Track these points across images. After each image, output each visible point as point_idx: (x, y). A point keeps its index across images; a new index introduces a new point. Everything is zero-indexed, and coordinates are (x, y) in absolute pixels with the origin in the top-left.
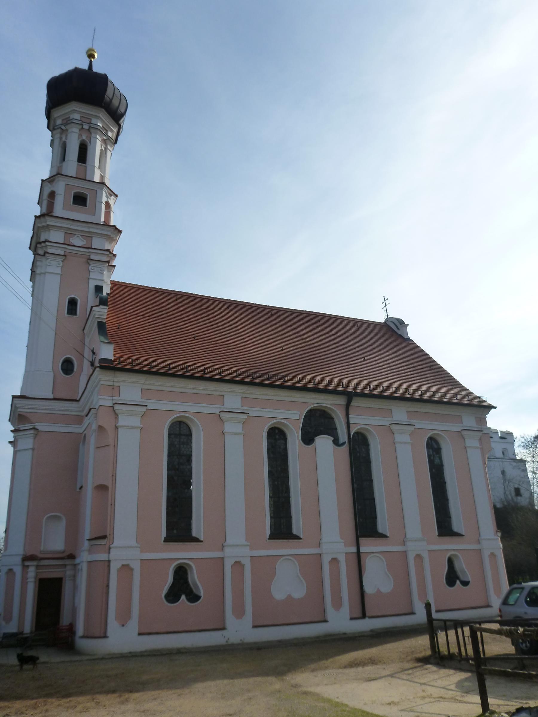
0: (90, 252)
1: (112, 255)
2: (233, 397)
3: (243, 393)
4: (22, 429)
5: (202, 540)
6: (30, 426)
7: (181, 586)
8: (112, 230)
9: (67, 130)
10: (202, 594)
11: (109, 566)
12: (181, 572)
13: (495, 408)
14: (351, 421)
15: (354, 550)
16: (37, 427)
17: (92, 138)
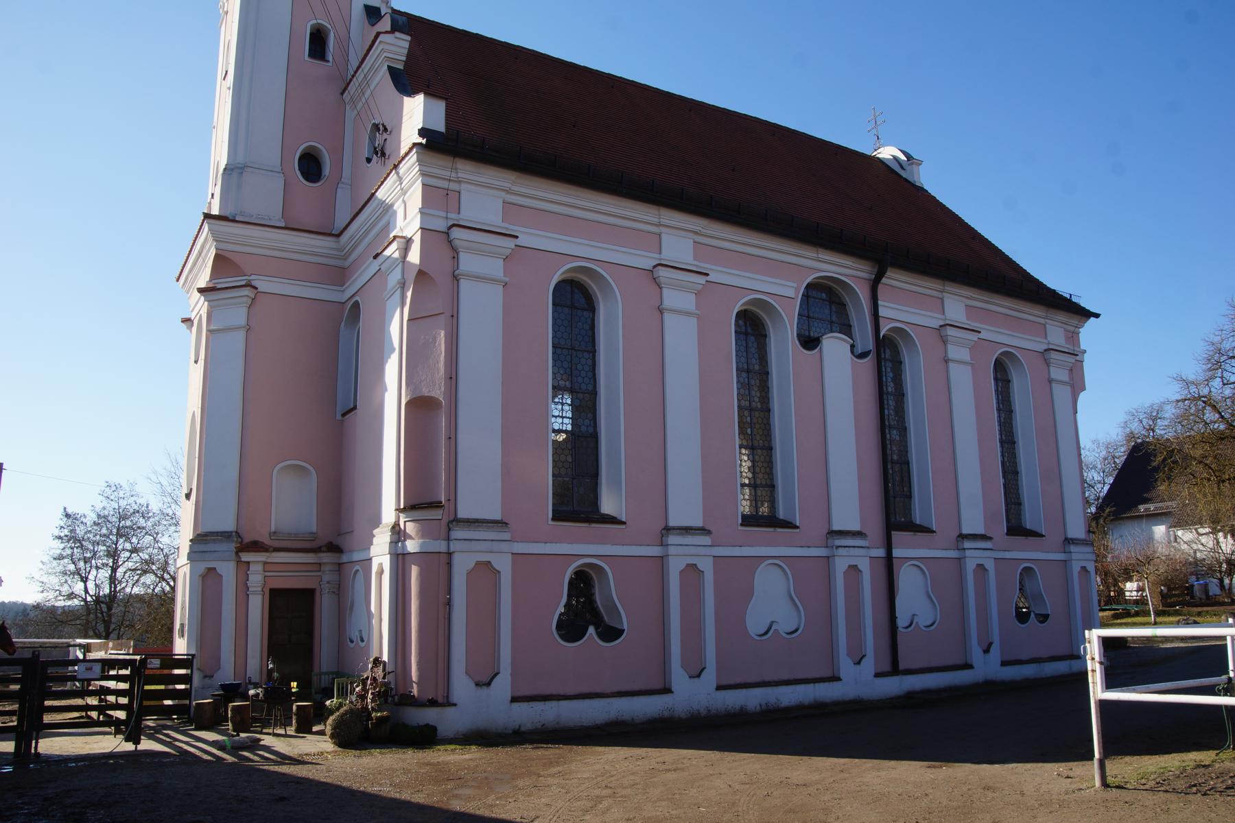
2: (679, 237)
3: (696, 233)
6: (241, 281)
7: (584, 611)
10: (625, 627)
11: (449, 564)
12: (583, 582)
13: (1097, 316)
14: (882, 312)
15: (881, 552)
16: (254, 283)
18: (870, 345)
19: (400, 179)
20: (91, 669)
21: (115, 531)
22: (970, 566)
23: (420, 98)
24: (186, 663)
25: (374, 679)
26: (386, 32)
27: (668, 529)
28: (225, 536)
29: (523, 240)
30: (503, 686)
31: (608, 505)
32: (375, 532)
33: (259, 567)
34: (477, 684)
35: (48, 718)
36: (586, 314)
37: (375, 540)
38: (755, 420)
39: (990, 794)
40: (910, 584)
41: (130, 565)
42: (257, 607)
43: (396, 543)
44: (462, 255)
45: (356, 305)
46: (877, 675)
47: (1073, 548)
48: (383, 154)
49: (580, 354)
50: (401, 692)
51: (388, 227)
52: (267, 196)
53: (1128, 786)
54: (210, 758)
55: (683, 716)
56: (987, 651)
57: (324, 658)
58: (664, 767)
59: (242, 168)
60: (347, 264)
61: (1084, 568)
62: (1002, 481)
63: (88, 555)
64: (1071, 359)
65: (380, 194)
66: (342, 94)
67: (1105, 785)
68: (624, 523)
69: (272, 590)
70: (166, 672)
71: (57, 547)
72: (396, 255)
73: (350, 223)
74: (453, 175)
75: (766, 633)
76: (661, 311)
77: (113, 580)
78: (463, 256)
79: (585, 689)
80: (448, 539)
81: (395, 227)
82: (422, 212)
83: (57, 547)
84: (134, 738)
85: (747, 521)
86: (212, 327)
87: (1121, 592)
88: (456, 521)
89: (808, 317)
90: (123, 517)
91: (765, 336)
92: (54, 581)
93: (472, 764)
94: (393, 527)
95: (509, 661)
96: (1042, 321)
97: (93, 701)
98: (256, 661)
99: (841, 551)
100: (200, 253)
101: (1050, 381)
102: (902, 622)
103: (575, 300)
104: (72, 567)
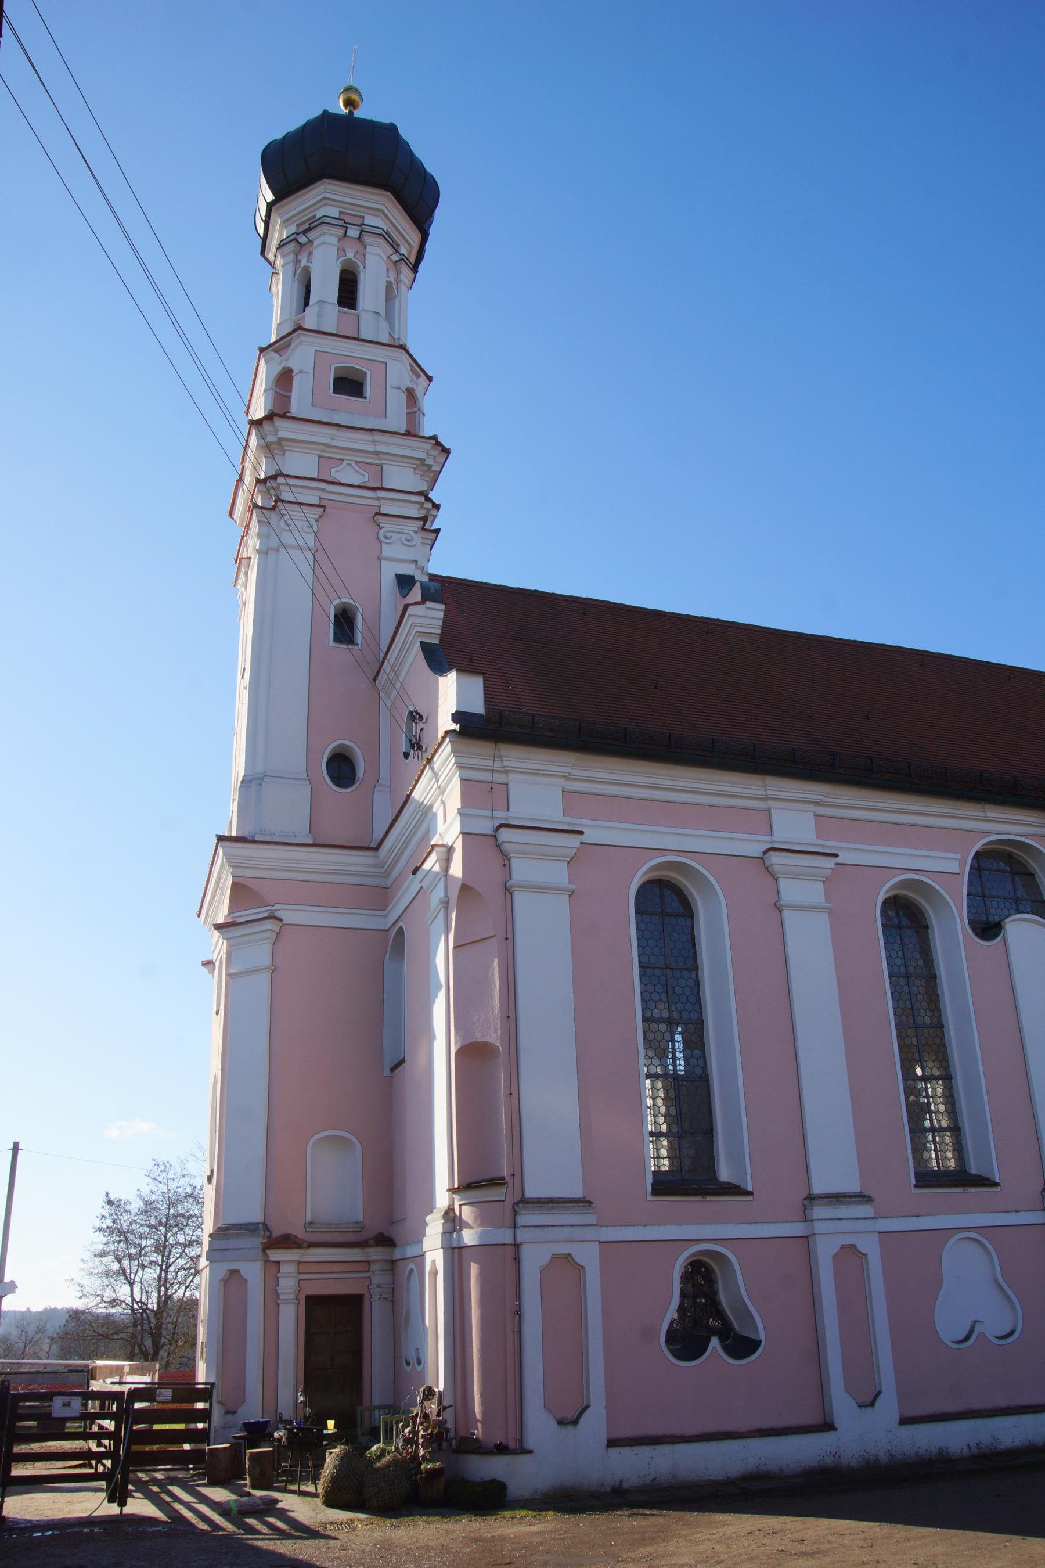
0: (378, 499)
1: (430, 506)
2: (796, 812)
3: (817, 804)
5: (750, 1189)
6: (262, 912)
7: (704, 1318)
8: (429, 446)
9: (310, 242)
10: (762, 1337)
11: (517, 1259)
12: (701, 1277)
17: (367, 256)
19: (436, 775)
21: (164, 1220)
23: (453, 676)
24: (206, 1395)
25: (426, 1416)
27: (811, 1198)
28: (250, 1228)
29: (593, 834)
30: (595, 1425)
31: (725, 1174)
32: (428, 1218)
34: (561, 1422)
35: (18, 1470)
36: (681, 921)
37: (428, 1229)
38: (923, 1041)
42: (290, 1319)
43: (451, 1233)
44: (514, 861)
45: (401, 931)
48: (420, 747)
49: (677, 974)
50: (462, 1434)
51: (428, 834)
52: (291, 809)
54: (206, 1527)
55: (854, 1463)
58: (802, 1548)
59: (262, 779)
63: (133, 1251)
65: (416, 795)
66: (375, 680)
68: (750, 1193)
69: (308, 1298)
70: (185, 1406)
71: (99, 1241)
72: (437, 868)
74: (497, 764)
75: (967, 1338)
76: (779, 909)
77: (162, 1282)
78: (515, 863)
79: (711, 1427)
80: (515, 1227)
82: (461, 813)
83: (99, 1241)
84: (118, 1495)
85: (663, 1185)
86: (232, 971)
88: (524, 1202)
89: (984, 896)
90: (171, 1204)
91: (927, 927)
93: (536, 1539)
94: (446, 1213)
98: (291, 1397)
100: (217, 883)
103: (666, 905)
104: (116, 1266)
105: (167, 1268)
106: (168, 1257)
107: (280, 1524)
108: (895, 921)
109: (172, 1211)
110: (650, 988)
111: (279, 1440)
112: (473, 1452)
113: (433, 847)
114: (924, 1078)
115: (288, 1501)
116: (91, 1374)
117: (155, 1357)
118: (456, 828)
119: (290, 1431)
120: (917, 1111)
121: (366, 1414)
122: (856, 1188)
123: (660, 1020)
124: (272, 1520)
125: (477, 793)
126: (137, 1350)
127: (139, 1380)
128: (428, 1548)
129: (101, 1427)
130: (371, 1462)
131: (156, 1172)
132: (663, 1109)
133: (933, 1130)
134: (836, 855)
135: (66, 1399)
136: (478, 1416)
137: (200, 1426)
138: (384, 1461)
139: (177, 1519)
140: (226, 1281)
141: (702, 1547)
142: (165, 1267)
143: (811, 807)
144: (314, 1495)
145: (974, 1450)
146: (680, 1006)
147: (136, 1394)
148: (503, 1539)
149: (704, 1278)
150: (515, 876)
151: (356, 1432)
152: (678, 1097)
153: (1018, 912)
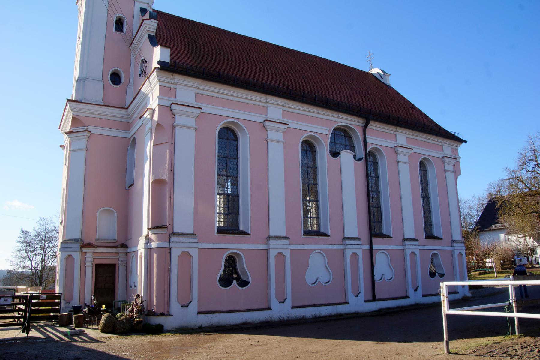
2: (276, 108)
3: (283, 106)
4: (74, 131)
7: (231, 274)
10: (250, 281)
11: (170, 253)
12: (231, 261)
13: (466, 142)
14: (368, 140)
15: (368, 247)
16: (89, 130)
18: (363, 155)
19: (150, 83)
20: (7, 300)
22: (408, 253)
24: (59, 297)
25: (137, 304)
26: (147, 19)
27: (269, 237)
28: (76, 241)
29: (204, 110)
30: (194, 307)
31: (241, 228)
33: (91, 255)
34: (182, 306)
36: (234, 142)
38: (310, 189)
39: (397, 357)
40: (380, 260)
41: (50, 253)
42: (90, 273)
44: (176, 116)
45: (134, 139)
46: (366, 301)
47: (455, 244)
48: (145, 73)
49: (231, 160)
50: (149, 309)
51: (146, 104)
52: (96, 91)
53: (460, 353)
54: (59, 340)
55: (276, 320)
56: (416, 290)
57: (120, 294)
58: (258, 344)
59: (85, 79)
60: (131, 121)
61: (460, 253)
62: (423, 215)
63: (32, 249)
64: (455, 161)
65: (143, 90)
67: (449, 353)
68: (250, 234)
69: (97, 265)
70: (51, 301)
72: (149, 117)
73: (131, 103)
74: (173, 81)
75: (315, 283)
77: (43, 260)
81: (149, 104)
82: (159, 97)
84: (26, 330)
85: (220, 231)
87: (484, 263)
92: (18, 260)
94: (146, 237)
95: (197, 295)
96: (441, 144)
97: (16, 314)
98: (89, 298)
99: (349, 247)
100: (67, 117)
101: (445, 171)
102: (377, 278)
103: (229, 136)
104: (25, 255)
105: (45, 255)
106: (45, 252)
107: (85, 338)
108: (305, 148)
109: (47, 235)
110: (221, 164)
111: (85, 312)
112: (152, 315)
113: (148, 109)
114: (309, 201)
115: (88, 331)
116: (16, 291)
117: (40, 285)
118: (157, 103)
119: (89, 309)
120: (306, 212)
121: (116, 303)
122: (284, 235)
123: (223, 175)
124: (82, 337)
125: (165, 91)
126: (33, 283)
127: (35, 293)
128: (136, 345)
129: (19, 308)
130: (117, 318)
131: (41, 222)
132: (222, 205)
133: (311, 218)
134: (288, 124)
135: (6, 298)
136: (155, 304)
137: (57, 307)
138: (122, 318)
139: (48, 337)
140: (67, 259)
141: (227, 344)
142: (44, 255)
143: (281, 107)
144: (98, 329)
145: (314, 316)
146: (231, 171)
147: (33, 297)
148: (162, 342)
149: (232, 261)
150: (176, 122)
151: (112, 309)
152: (228, 201)
153: (345, 149)
